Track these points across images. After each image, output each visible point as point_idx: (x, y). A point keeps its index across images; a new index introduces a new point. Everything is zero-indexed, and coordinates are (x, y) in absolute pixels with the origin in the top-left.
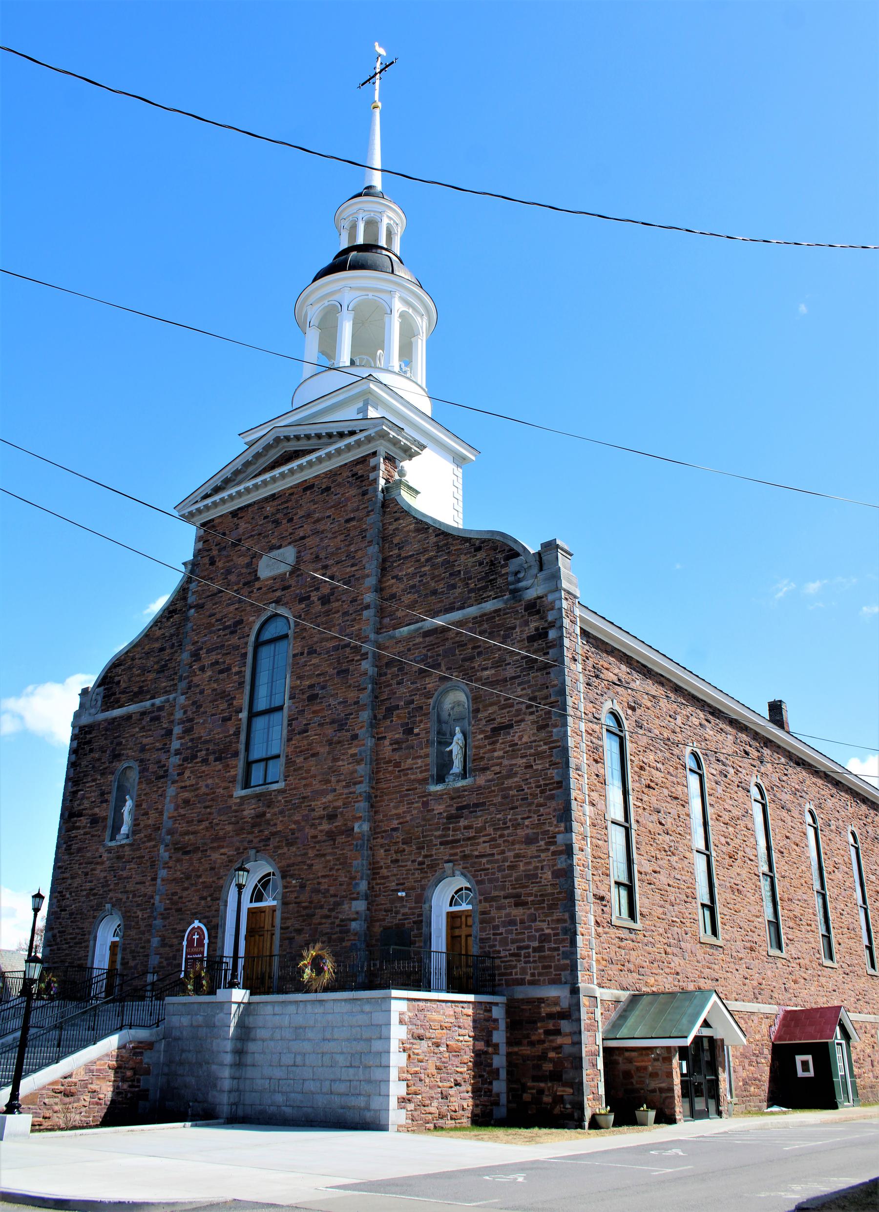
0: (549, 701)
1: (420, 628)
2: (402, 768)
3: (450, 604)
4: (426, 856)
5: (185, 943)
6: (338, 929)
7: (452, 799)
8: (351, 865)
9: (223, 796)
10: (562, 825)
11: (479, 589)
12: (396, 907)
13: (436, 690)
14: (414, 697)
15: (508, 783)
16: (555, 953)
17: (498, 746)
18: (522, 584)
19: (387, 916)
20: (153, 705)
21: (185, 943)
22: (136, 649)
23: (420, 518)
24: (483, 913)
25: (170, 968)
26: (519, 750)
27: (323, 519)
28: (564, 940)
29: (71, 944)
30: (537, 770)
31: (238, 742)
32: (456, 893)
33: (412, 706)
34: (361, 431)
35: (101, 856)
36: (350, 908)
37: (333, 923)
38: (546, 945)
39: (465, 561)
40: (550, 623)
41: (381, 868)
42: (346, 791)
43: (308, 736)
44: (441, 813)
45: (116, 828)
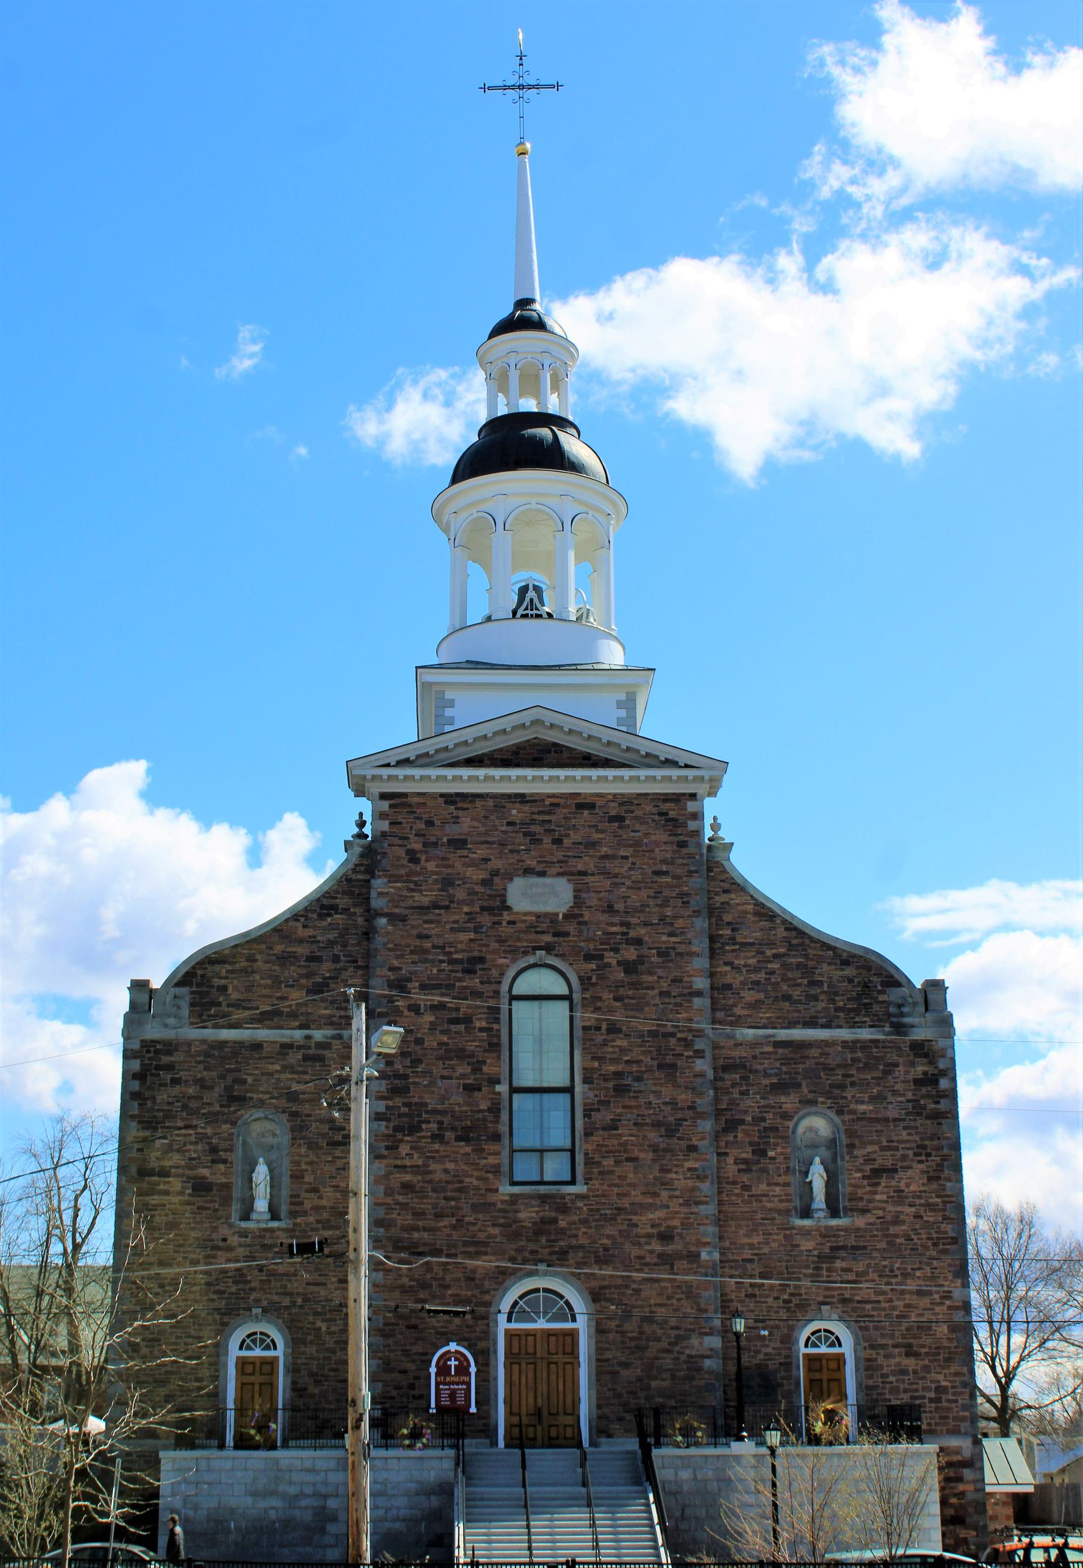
0: (940, 1153)
1: (773, 1036)
2: (753, 1193)
3: (811, 1017)
5: (433, 1370)
7: (823, 1236)
8: (698, 1296)
9: (478, 1188)
10: (959, 1281)
11: (850, 1010)
13: (796, 1113)
14: (765, 1115)
15: (892, 1230)
16: (954, 1405)
17: (880, 1189)
18: (907, 1020)
20: (308, 1037)
21: (433, 1370)
22: (255, 946)
23: (761, 900)
24: (868, 1360)
26: (907, 1197)
27: (614, 857)
28: (962, 1393)
30: (927, 1222)
31: (497, 1122)
32: (249, 1336)
33: (763, 1124)
35: (225, 1240)
36: (701, 1343)
37: (677, 1359)
38: (944, 1397)
39: (826, 971)
40: (940, 1071)
42: (684, 1210)
43: (620, 1135)
44: (810, 1251)
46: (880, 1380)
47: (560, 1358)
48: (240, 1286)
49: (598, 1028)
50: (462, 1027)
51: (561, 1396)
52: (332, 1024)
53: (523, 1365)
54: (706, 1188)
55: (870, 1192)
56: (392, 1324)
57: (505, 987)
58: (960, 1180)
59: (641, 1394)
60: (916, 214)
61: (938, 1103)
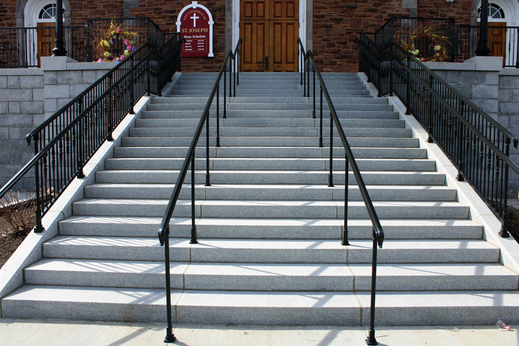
5: (178, 23)
12: (442, 11)
21: (178, 23)
32: (46, 8)
36: (400, 5)
47: (284, 20)
51: (284, 48)
53: (255, 25)
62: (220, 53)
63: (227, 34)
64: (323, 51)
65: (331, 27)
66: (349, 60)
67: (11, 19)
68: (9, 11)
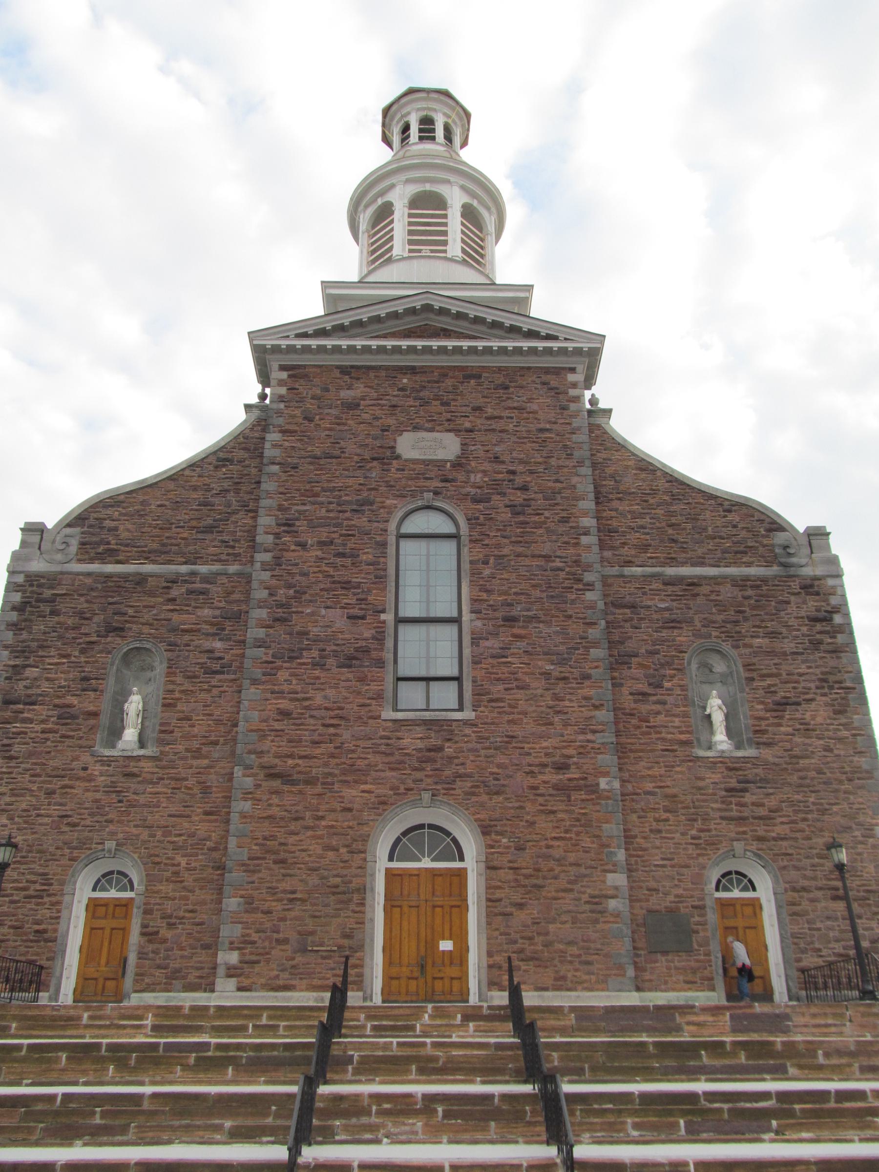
4: (701, 830)
6: (587, 907)
12: (664, 886)
17: (784, 722)
18: (794, 560)
19: (652, 895)
25: (267, 944)
29: (15, 898)
31: (382, 650)
32: (104, 876)
34: (566, 339)
35: (85, 769)
41: (635, 837)
45: (117, 732)
46: (806, 926)
48: (96, 819)
49: (486, 563)
50: (349, 561)
52: (220, 561)
53: (405, 909)
54: (604, 715)
55: (773, 725)
56: (258, 858)
57: (392, 526)
58: (866, 713)
59: (539, 939)
60: (515, 983)
61: (835, 637)
62: (358, 954)
63: (368, 925)
64: (502, 951)
65: (511, 914)
66: (537, 963)
67: (55, 895)
68: (55, 884)
